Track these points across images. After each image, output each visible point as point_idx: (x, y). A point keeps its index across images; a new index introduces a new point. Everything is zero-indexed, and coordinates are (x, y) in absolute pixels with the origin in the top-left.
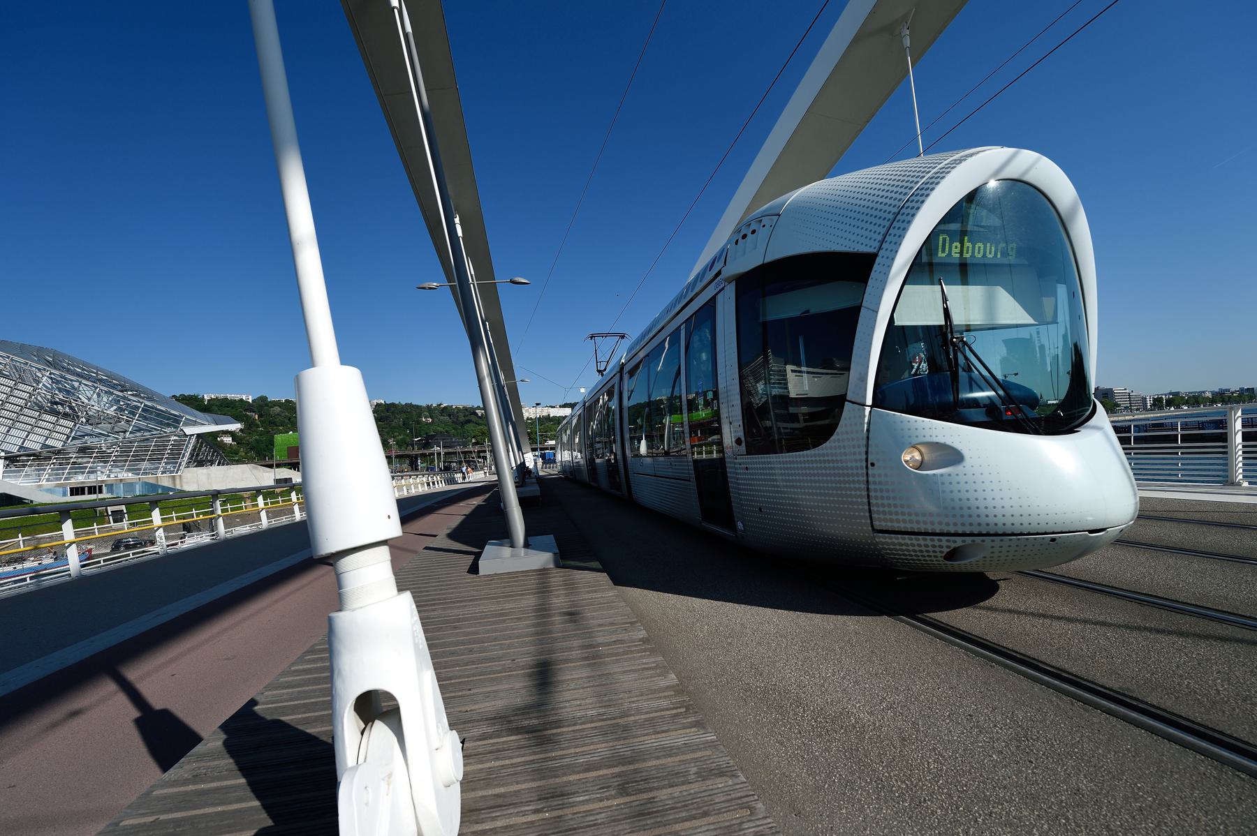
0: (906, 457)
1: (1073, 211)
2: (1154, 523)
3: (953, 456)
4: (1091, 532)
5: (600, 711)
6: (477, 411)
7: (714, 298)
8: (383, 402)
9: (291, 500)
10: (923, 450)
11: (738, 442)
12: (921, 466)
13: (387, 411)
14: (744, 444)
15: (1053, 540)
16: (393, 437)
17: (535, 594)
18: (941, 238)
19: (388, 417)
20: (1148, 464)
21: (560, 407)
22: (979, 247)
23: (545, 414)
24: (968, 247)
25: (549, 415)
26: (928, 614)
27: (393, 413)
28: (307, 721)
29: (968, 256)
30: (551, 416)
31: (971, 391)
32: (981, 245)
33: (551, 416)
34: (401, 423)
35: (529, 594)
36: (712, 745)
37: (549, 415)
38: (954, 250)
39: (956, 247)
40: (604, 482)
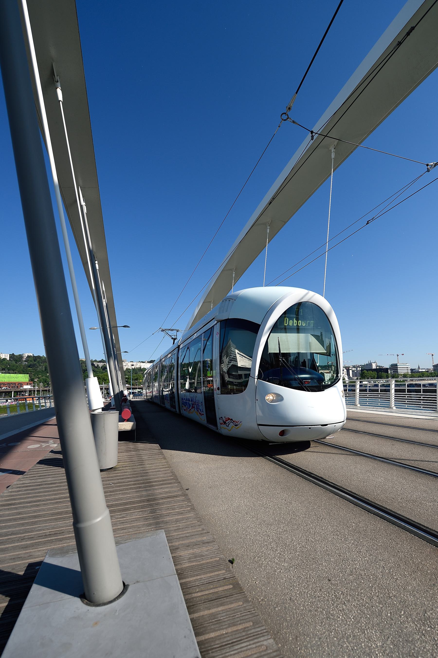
0: (267, 398)
1: (330, 312)
2: (393, 427)
3: (280, 398)
4: (322, 425)
5: (169, 538)
6: (94, 363)
7: (213, 326)
8: (32, 355)
9: (242, 389)
10: (273, 395)
11: (218, 389)
12: (273, 401)
13: (35, 361)
14: (220, 390)
15: (310, 428)
16: (38, 378)
17: (142, 507)
18: (285, 319)
19: (34, 365)
20: (386, 403)
21: (148, 362)
22: (300, 322)
23: (138, 366)
24: (295, 322)
25: (140, 367)
26: (277, 456)
27: (38, 362)
28: (44, 466)
29: (300, 325)
30: (142, 368)
31: (298, 374)
32: (295, 325)
33: (142, 368)
34: (44, 369)
35: (135, 508)
36: (184, 498)
37: (140, 367)
38: (290, 323)
39: (291, 322)
40: (168, 405)
